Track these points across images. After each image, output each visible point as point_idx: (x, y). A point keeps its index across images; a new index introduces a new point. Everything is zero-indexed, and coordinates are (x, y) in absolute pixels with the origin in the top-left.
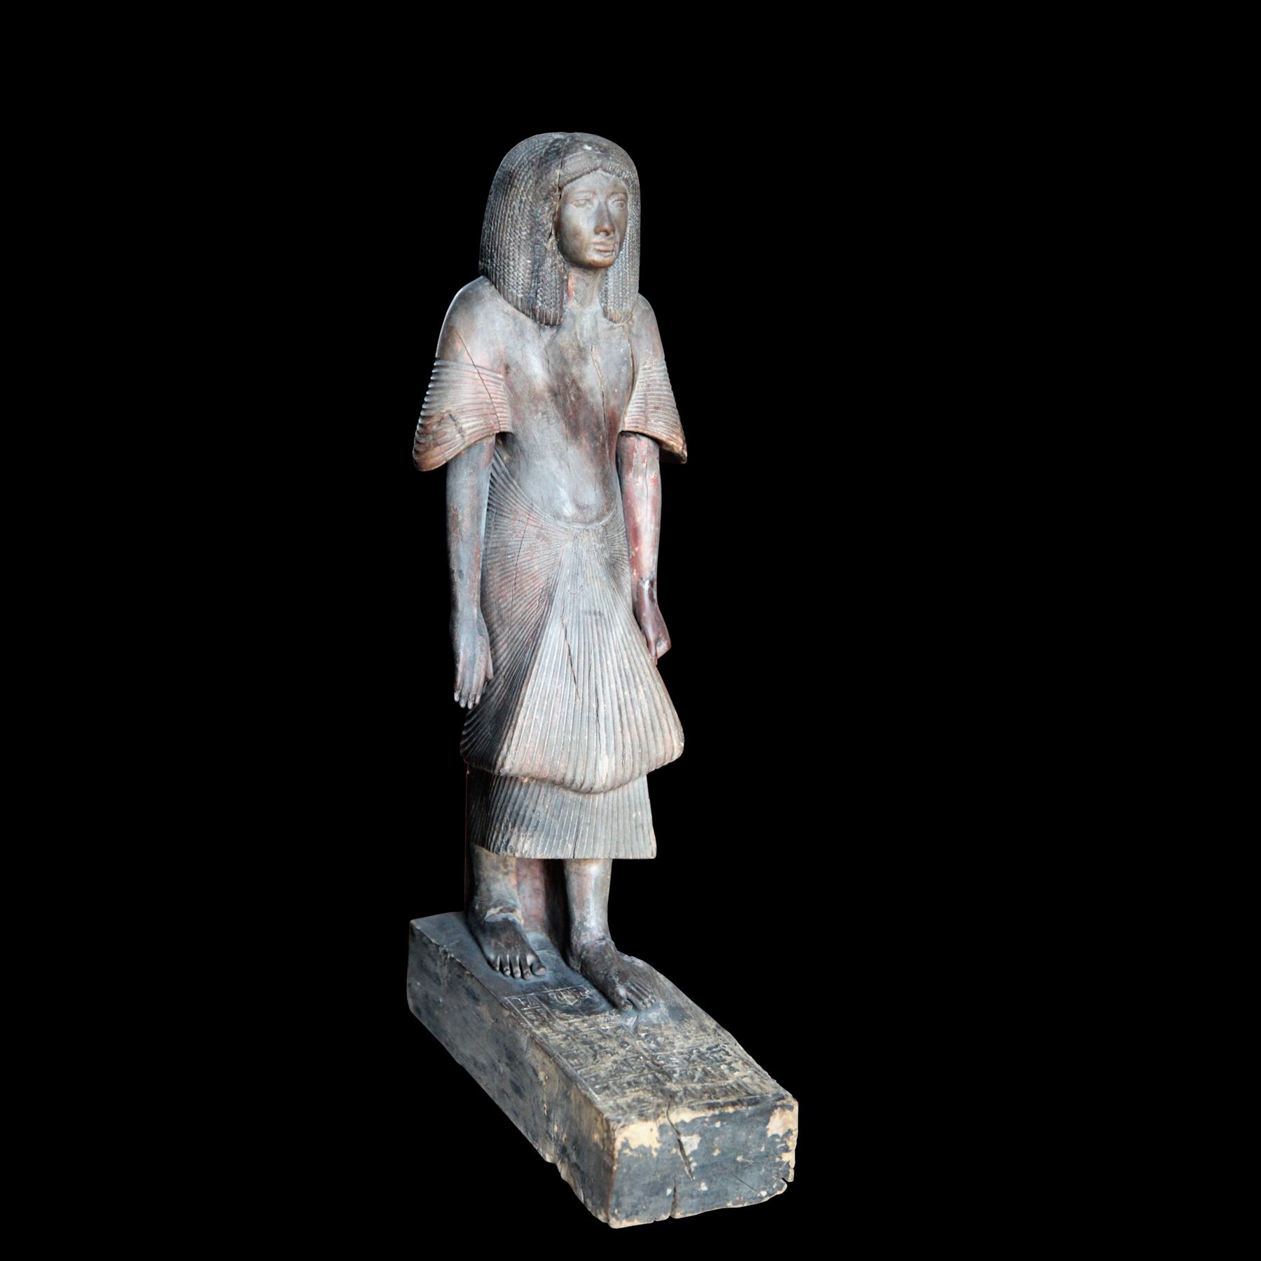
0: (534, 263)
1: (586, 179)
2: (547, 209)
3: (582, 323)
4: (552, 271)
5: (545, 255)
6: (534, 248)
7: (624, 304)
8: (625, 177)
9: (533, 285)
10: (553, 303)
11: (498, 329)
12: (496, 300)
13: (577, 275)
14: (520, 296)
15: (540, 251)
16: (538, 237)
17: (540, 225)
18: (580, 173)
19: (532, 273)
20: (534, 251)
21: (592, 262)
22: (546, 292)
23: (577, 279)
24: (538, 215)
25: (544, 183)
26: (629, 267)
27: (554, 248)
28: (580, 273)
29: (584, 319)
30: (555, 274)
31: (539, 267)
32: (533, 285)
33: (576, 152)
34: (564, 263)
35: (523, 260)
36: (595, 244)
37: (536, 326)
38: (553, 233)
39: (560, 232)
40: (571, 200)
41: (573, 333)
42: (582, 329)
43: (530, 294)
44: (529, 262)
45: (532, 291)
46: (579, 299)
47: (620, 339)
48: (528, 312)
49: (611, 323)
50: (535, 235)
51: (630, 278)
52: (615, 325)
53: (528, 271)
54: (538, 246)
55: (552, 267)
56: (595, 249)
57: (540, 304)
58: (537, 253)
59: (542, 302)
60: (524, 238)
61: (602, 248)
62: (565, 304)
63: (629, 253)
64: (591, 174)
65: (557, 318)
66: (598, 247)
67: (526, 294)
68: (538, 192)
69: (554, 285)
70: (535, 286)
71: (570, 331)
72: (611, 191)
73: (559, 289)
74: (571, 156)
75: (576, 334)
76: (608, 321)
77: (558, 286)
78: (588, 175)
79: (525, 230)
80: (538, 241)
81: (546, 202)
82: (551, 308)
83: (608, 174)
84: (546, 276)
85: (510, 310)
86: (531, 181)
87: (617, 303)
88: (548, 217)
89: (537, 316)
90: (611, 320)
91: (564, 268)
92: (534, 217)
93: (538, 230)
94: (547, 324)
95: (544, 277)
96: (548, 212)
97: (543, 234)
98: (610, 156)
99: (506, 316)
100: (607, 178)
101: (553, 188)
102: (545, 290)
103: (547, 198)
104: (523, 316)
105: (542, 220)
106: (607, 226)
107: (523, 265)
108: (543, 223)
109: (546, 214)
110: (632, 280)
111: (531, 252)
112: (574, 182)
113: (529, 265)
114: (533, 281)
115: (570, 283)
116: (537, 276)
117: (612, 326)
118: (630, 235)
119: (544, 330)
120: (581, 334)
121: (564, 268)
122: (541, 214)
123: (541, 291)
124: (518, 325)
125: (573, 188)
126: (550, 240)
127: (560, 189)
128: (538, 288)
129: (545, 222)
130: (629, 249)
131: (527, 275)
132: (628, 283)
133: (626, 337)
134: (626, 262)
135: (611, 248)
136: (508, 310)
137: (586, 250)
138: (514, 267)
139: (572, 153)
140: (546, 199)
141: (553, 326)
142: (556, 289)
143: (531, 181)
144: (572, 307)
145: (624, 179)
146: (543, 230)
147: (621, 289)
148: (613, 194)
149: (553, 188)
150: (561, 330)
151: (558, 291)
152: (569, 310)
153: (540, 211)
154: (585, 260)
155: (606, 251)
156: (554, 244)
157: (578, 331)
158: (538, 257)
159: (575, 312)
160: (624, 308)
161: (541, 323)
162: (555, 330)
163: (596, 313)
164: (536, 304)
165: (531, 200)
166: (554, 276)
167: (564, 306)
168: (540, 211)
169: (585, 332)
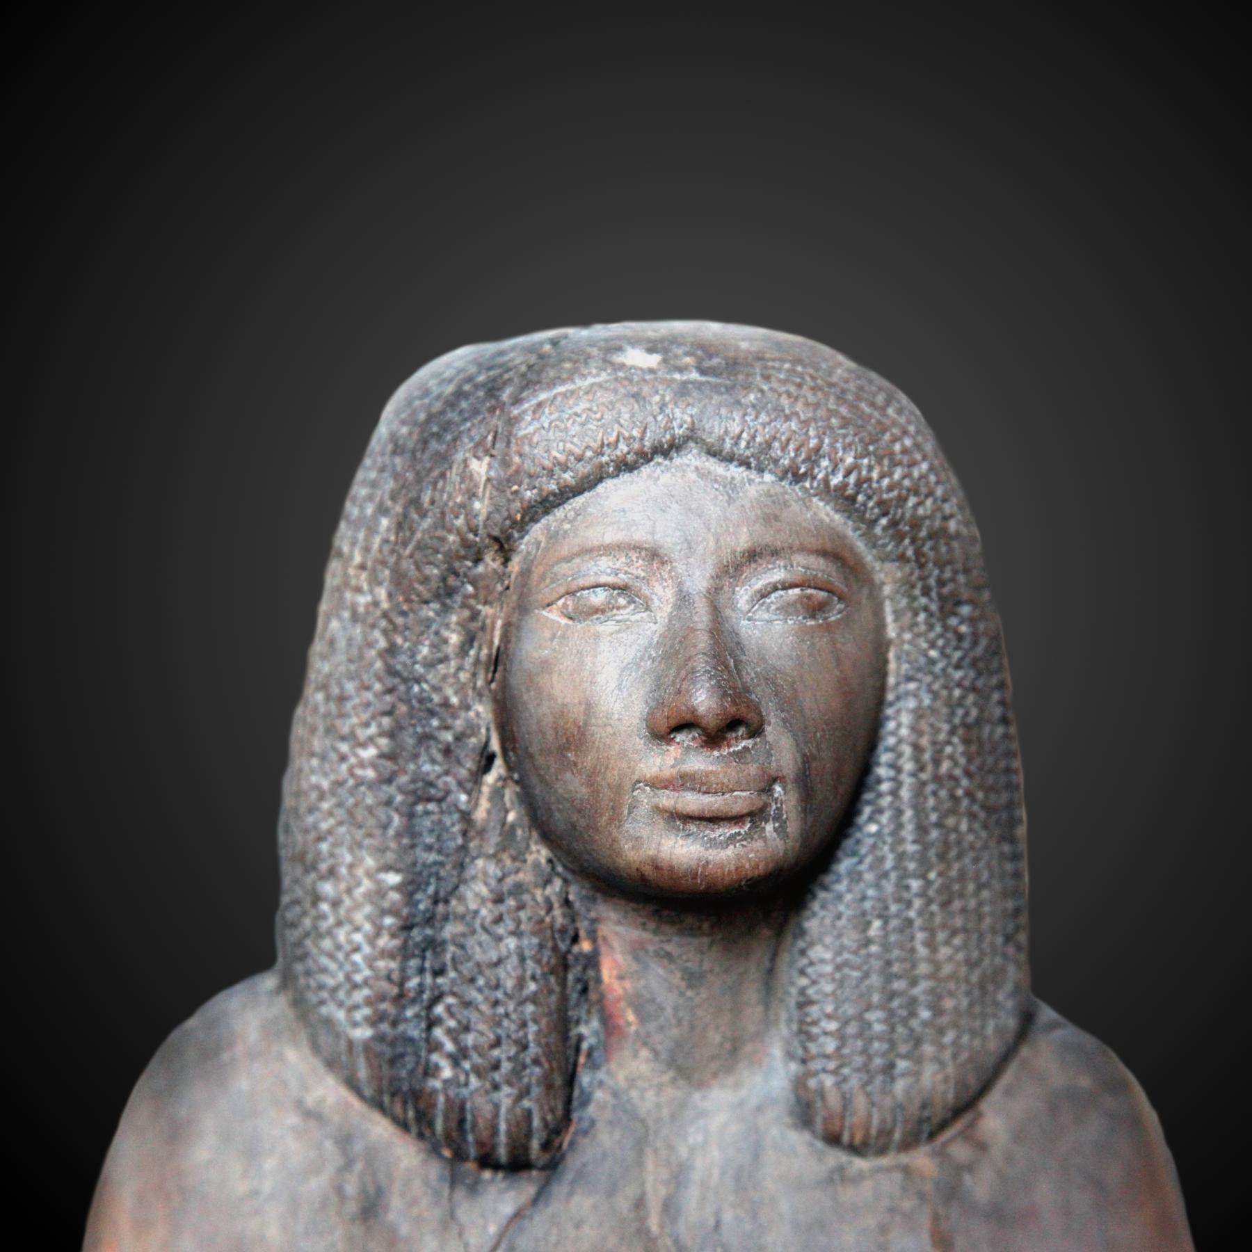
0: (410, 888)
1: (614, 492)
2: (454, 638)
3: (683, 1152)
4: (499, 920)
5: (464, 848)
6: (411, 815)
7: (902, 1065)
8: (836, 480)
9: (413, 983)
10: (506, 1066)
11: (267, 1187)
12: (281, 1057)
13: (635, 934)
14: (363, 1033)
15: (440, 830)
16: (427, 767)
17: (432, 713)
18: (584, 469)
19: (407, 927)
20: (410, 830)
21: (648, 871)
22: (474, 1016)
23: (637, 951)
24: (419, 668)
25: (427, 523)
26: (922, 894)
27: (511, 817)
28: (644, 926)
29: (695, 1138)
30: (517, 933)
31: (436, 900)
32: (413, 983)
33: (570, 379)
34: (565, 881)
35: (369, 874)
36: (658, 784)
37: (435, 1170)
38: (495, 746)
39: (514, 740)
40: (545, 594)
41: (623, 1204)
42: (679, 1176)
43: (402, 1027)
44: (393, 879)
45: (409, 1013)
46: (662, 1042)
47: (883, 1229)
48: (398, 1109)
49: (836, 1157)
50: (415, 757)
51: (931, 945)
52: (860, 1164)
53: (388, 921)
54: (431, 806)
55: (499, 900)
56: (658, 810)
57: (447, 1073)
58: (429, 840)
59: (455, 1060)
60: (370, 774)
61: (692, 801)
62: (595, 1067)
63: (922, 829)
64: (646, 470)
65: (529, 1135)
66: (667, 799)
67: (385, 1027)
68: (407, 566)
69: (509, 984)
70: (421, 989)
71: (612, 1192)
72: (743, 541)
73: (534, 999)
74: (543, 396)
75: (640, 1204)
76: (820, 1145)
77: (532, 987)
78: (625, 477)
79: (915, 695)
80: (431, 784)
81: (446, 609)
82: (496, 1087)
83: (736, 471)
84: (471, 942)
85: (331, 1100)
86: (385, 522)
87: (859, 1060)
88: (464, 676)
89: (439, 1125)
90: (833, 1139)
91: (567, 903)
92: (405, 681)
93: (425, 738)
94: (487, 1161)
95: (462, 947)
96: (463, 651)
97: (447, 751)
98: (748, 388)
99: (313, 1123)
100: (731, 487)
101: (465, 544)
102: (467, 1004)
103: (451, 592)
104: (380, 1129)
105: (436, 689)
106: (703, 699)
107: (368, 896)
108: (446, 704)
109: (453, 664)
110: (944, 952)
111: (399, 835)
112: (559, 513)
113: (395, 896)
114: (414, 963)
115: (607, 973)
116: (434, 945)
117: (841, 1169)
118: (917, 748)
119: (474, 1189)
120: (670, 1208)
121: (567, 903)
122: (430, 665)
123: (449, 1009)
124: (359, 1166)
125: (554, 537)
126: (490, 778)
127: (504, 547)
128: (436, 999)
129: (454, 700)
130: (919, 810)
131: (384, 941)
132: (923, 968)
133: (925, 1221)
134: (905, 875)
135: (741, 800)
136: (322, 1101)
137: (616, 818)
138: (336, 904)
139: (552, 384)
140: (444, 594)
141: (517, 1165)
142: (522, 1003)
143: (385, 522)
144: (632, 1082)
145: (825, 490)
146: (448, 737)
147: (876, 998)
148: (752, 556)
149: (465, 544)
150: (560, 1190)
151: (530, 1008)
152: (615, 1094)
153: (425, 651)
154: (621, 862)
155: (714, 819)
156: (509, 794)
157: (656, 1193)
158: (432, 857)
159: (647, 1101)
160: (900, 1087)
161: (459, 1156)
162: (530, 1190)
163: (759, 1109)
164: (431, 1071)
165: (385, 605)
166: (512, 943)
167: (585, 1079)
168: (425, 651)
169: (691, 1198)
